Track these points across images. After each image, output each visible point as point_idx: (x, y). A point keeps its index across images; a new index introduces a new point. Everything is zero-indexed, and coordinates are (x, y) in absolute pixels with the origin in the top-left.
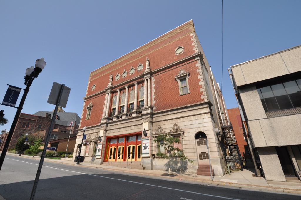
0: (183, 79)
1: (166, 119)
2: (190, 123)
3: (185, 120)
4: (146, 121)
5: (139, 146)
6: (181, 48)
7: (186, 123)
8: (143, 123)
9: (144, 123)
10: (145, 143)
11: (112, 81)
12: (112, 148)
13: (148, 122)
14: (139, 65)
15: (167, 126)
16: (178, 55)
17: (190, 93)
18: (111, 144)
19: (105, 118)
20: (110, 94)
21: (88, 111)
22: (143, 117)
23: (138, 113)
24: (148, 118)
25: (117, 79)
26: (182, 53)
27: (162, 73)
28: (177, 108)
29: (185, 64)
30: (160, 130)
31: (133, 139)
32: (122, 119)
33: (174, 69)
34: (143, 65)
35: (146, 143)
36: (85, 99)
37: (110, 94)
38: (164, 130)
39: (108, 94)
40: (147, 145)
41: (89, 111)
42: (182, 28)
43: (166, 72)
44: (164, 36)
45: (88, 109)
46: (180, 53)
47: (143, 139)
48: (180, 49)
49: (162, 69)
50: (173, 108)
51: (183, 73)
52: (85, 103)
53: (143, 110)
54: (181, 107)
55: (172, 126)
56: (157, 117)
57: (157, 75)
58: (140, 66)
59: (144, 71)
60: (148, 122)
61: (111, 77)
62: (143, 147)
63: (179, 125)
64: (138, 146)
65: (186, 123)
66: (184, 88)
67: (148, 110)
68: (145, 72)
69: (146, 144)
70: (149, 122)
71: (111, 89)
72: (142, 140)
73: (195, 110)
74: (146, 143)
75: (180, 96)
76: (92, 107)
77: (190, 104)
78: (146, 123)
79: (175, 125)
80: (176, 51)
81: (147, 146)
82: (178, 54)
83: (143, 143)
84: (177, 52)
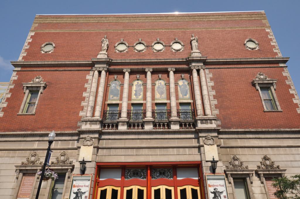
0: (266, 87)
1: (246, 145)
2: (291, 158)
3: (282, 153)
4: (89, 143)
5: (128, 191)
6: (125, 45)
7: (284, 158)
8: (80, 148)
9: (82, 147)
10: (78, 186)
11: (107, 50)
12: (105, 190)
13: (92, 146)
14: (46, 43)
15: (250, 158)
16: (117, 52)
17: (34, 115)
18: (100, 179)
19: (96, 121)
20: (103, 73)
21: (28, 95)
22: (82, 136)
23: (105, 126)
24: (93, 139)
25: (46, 51)
26: (125, 52)
27: (74, 70)
28: (267, 130)
29: (265, 67)
30: (237, 163)
31: (166, 175)
32: (117, 131)
33: (247, 68)
34: (54, 45)
35: (82, 186)
36: (16, 66)
37: (103, 73)
38: (245, 165)
39: (100, 72)
40: (83, 190)
41: (30, 95)
42: (249, 16)
43: (232, 68)
44: (92, 17)
45: (28, 91)
46: (47, 52)
47: (74, 178)
48: (123, 45)
49: (226, 62)
50: (260, 130)
51: (38, 83)
52: (17, 74)
53: (199, 122)
54: (274, 130)
55: (260, 159)
56: (227, 138)
57: (215, 68)
58: (121, 45)
59: (96, 56)
60: (92, 146)
61: (106, 43)
62: (74, 193)
63: (273, 158)
64: (126, 189)
65: (284, 158)
66: (271, 101)
67: (211, 123)
68: (98, 59)
69: (81, 188)
70: (94, 147)
71: (107, 64)
72: (73, 180)
73: (256, 139)
74: (82, 186)
75: (18, 115)
76: (45, 88)
77: (289, 128)
78: (210, 146)
79: (266, 158)
80: (43, 46)
81: (83, 192)
82: (137, 50)
83: (75, 186)
84: (136, 47)
